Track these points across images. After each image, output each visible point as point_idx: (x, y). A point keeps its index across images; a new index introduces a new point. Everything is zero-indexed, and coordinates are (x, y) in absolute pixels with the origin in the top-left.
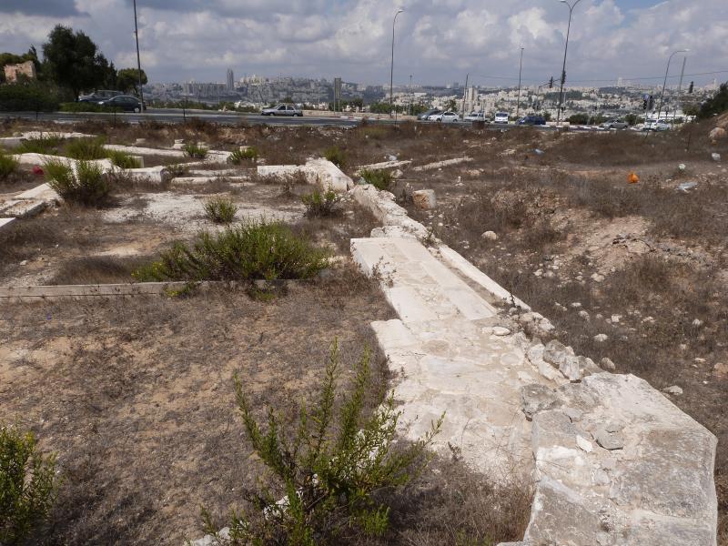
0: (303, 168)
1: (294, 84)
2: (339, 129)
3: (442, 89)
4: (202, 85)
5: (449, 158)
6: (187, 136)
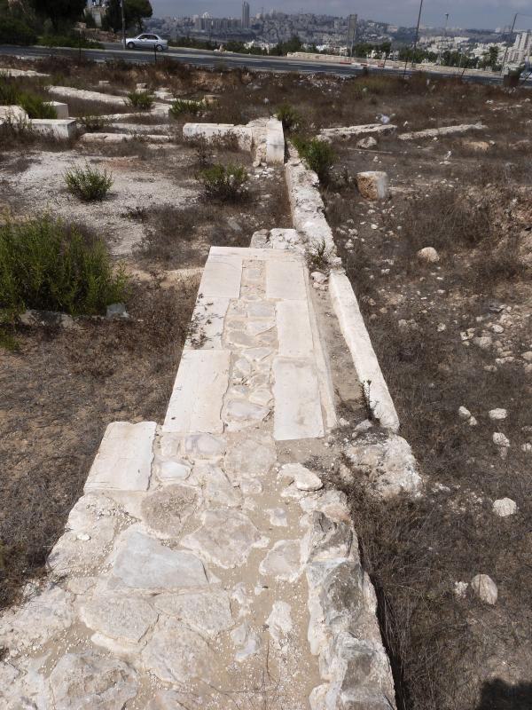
0: (239, 130)
1: (315, 22)
2: (334, 78)
3: (489, 33)
4: (215, 20)
5: (454, 124)
6: (158, 80)
